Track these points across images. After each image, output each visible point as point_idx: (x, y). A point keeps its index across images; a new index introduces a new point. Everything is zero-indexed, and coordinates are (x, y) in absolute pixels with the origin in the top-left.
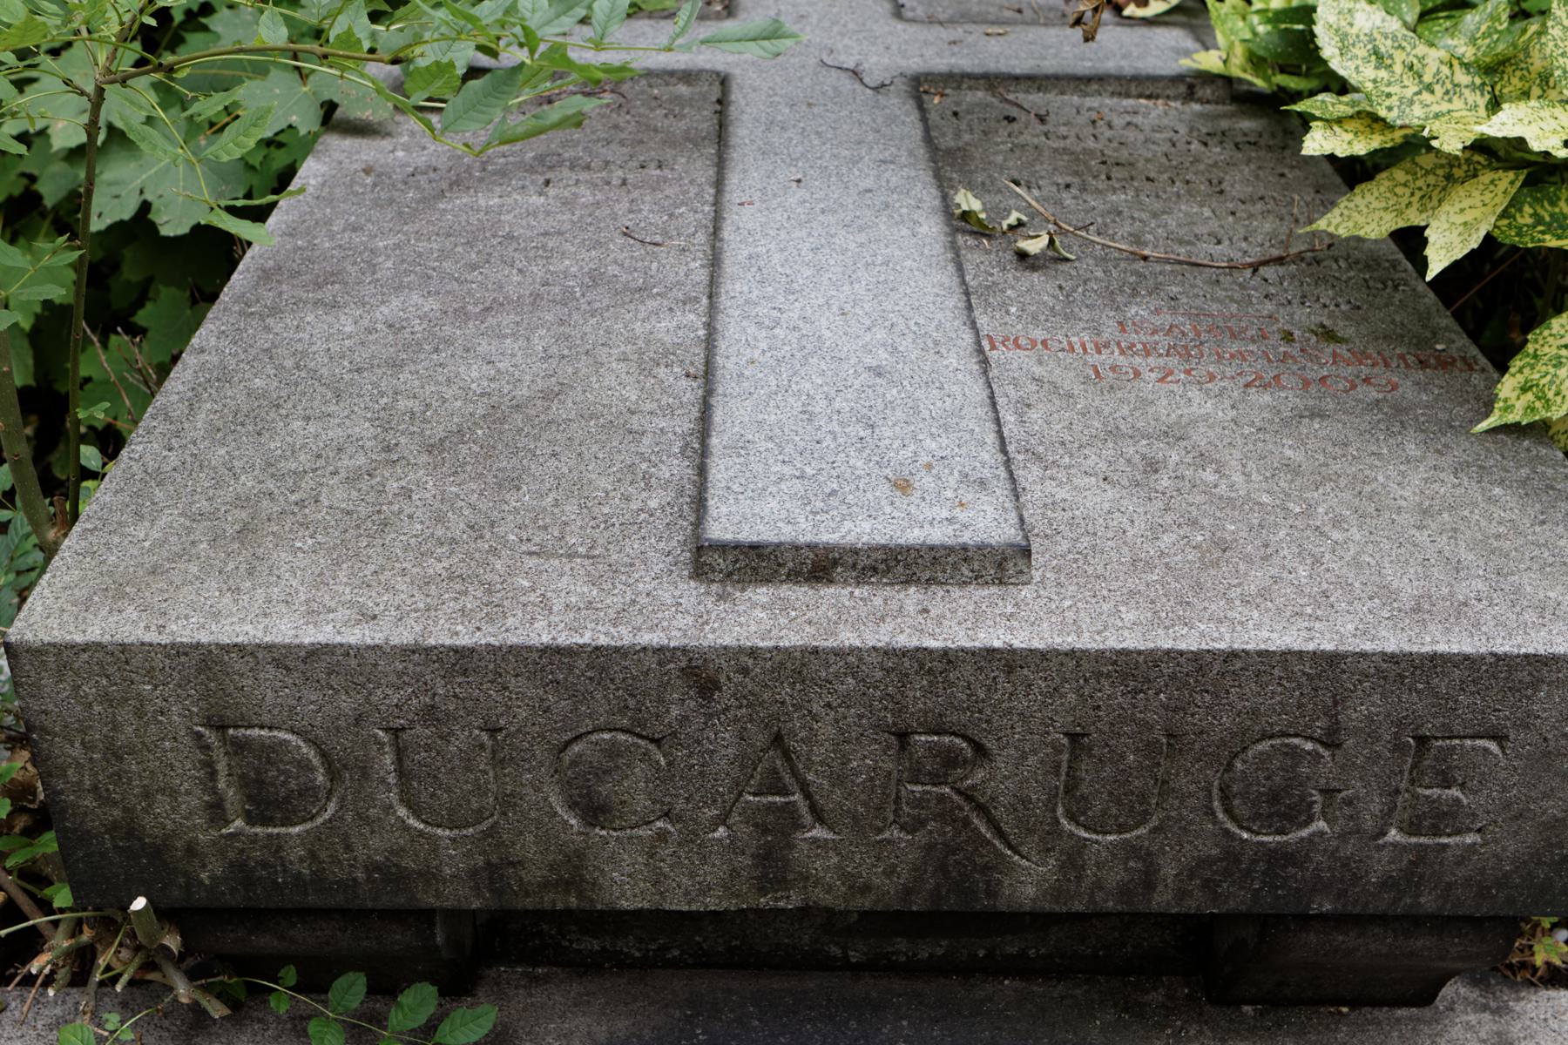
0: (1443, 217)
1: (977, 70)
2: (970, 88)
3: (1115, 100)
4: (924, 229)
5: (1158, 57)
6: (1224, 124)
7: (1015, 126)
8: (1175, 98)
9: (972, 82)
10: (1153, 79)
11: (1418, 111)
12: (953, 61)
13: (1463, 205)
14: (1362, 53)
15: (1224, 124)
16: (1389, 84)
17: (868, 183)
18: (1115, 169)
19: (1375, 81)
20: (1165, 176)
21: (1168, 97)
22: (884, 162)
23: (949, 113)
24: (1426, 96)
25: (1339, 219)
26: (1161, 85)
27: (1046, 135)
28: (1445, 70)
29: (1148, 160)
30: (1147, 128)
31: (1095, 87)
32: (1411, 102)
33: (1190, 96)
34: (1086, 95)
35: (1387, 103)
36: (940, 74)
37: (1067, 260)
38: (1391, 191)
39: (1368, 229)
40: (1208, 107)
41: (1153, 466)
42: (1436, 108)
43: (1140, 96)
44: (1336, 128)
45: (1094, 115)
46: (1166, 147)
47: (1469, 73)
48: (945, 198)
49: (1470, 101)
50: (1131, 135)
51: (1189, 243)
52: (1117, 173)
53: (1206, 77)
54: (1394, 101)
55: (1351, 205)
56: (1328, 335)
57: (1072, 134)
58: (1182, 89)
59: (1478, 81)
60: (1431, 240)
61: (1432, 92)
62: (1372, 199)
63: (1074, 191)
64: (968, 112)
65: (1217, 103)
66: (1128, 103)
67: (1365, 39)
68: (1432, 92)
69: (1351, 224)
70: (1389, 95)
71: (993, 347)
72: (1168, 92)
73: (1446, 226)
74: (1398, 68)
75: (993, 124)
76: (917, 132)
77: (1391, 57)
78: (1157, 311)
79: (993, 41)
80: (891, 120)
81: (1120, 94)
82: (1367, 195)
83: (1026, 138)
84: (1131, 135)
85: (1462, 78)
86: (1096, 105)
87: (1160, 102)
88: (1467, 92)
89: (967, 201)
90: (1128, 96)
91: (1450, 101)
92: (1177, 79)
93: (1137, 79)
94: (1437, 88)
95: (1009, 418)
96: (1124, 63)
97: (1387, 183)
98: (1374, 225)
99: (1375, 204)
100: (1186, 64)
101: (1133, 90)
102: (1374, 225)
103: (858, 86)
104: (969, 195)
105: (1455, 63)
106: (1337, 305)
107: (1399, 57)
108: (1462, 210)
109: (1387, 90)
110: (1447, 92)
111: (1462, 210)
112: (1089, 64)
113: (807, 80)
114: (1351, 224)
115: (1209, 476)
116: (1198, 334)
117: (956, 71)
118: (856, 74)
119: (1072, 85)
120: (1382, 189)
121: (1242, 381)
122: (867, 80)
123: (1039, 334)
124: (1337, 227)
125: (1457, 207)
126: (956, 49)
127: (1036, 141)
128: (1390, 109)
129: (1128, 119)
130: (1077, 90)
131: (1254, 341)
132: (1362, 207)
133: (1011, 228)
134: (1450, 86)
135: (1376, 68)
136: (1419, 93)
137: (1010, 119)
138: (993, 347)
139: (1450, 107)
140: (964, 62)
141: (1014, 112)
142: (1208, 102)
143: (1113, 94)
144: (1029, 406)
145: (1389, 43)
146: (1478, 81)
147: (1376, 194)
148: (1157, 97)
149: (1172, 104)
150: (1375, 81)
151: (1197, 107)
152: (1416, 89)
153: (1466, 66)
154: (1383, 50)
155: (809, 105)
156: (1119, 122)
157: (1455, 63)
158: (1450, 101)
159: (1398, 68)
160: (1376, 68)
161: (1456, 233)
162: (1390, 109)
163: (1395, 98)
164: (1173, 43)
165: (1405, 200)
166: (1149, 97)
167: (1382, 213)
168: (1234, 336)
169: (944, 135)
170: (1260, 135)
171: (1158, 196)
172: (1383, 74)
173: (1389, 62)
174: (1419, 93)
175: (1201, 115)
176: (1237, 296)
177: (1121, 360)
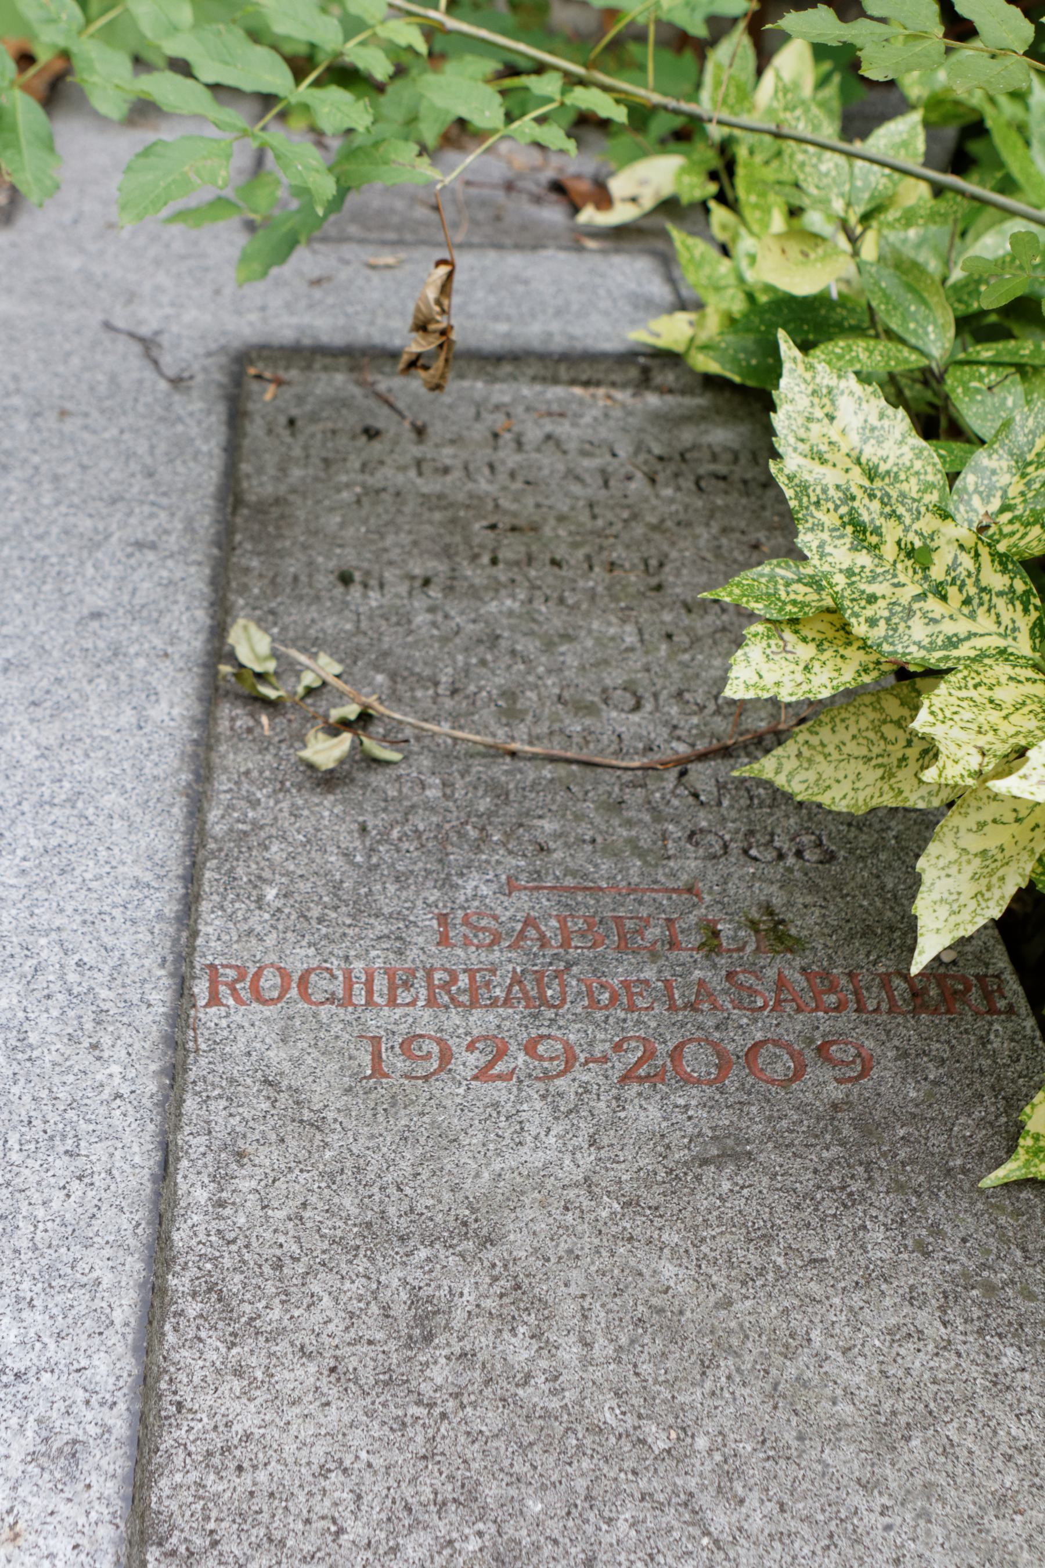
0: (949, 837)
1: (338, 340)
2: (325, 368)
3: (538, 388)
4: (158, 712)
5: (606, 314)
6: (687, 436)
7: (377, 446)
8: (624, 386)
9: (328, 361)
10: (592, 358)
11: (919, 631)
12: (307, 319)
13: (982, 816)
14: (830, 520)
15: (687, 436)
16: (873, 579)
17: (98, 598)
18: (511, 538)
19: (849, 573)
20: (580, 554)
21: (613, 384)
22: (140, 545)
23: (282, 420)
24: (932, 604)
25: (794, 763)
26: (602, 367)
27: (419, 463)
28: (967, 561)
29: (561, 519)
30: (572, 446)
31: (507, 368)
32: (910, 613)
33: (645, 382)
34: (494, 379)
35: (869, 612)
36: (282, 348)
37: (388, 763)
38: (877, 730)
39: (837, 792)
40: (670, 399)
41: (426, 1322)
42: (949, 628)
43: (573, 382)
44: (788, 635)
45: (499, 420)
46: (593, 490)
47: (1004, 571)
48: (219, 631)
49: (1006, 620)
50: (550, 463)
51: (591, 710)
52: (512, 549)
53: (670, 358)
54: (880, 609)
55: (814, 740)
56: (775, 933)
57: (458, 463)
58: (633, 373)
59: (1020, 586)
60: (927, 879)
61: (944, 598)
62: (847, 736)
63: (434, 592)
64: (314, 418)
65: (683, 392)
66: (556, 392)
67: (837, 495)
68: (944, 598)
69: (811, 776)
70: (872, 599)
71: (214, 999)
72: (614, 377)
73: (952, 855)
74: (889, 551)
75: (343, 441)
76: (208, 476)
77: (877, 531)
78: (511, 887)
79: (375, 277)
80: (180, 446)
81: (544, 380)
82: (841, 727)
83: (387, 475)
84: (550, 463)
85: (996, 580)
86: (506, 399)
87: (601, 391)
88: (1000, 603)
89: (251, 644)
90: (555, 381)
91: (972, 616)
92: (628, 357)
93: (567, 358)
94: (952, 591)
95: (194, 1189)
96: (555, 326)
97: (871, 715)
98: (846, 786)
99: (851, 748)
100: (639, 336)
101: (563, 372)
102: (846, 786)
103: (149, 374)
104: (253, 628)
105: (984, 551)
106: (799, 854)
107: (892, 532)
108: (981, 825)
109: (870, 589)
110: (967, 602)
111: (981, 825)
112: (503, 327)
113: (76, 361)
114: (811, 776)
115: (519, 1350)
116: (566, 944)
117: (307, 341)
118: (148, 346)
119: (474, 366)
120: (864, 723)
121: (619, 1066)
122: (166, 359)
123: (300, 958)
124: (791, 775)
125: (971, 822)
126: (317, 293)
127: (400, 479)
128: (872, 622)
129: (549, 427)
130: (480, 373)
131: (654, 956)
132: (830, 749)
133: (310, 691)
134: (972, 591)
135: (854, 549)
136: (922, 597)
137: (371, 434)
138: (214, 999)
139: (974, 628)
140: (325, 325)
141: (382, 418)
142: (671, 391)
143: (534, 379)
144: (240, 1155)
145: (875, 505)
146: (1020, 586)
147: (853, 730)
148: (598, 384)
149: (619, 395)
150: (849, 573)
151: (653, 400)
152: (918, 590)
153: (1002, 560)
154: (865, 517)
155: (63, 414)
156: (533, 434)
157: (984, 551)
158: (972, 616)
159: (889, 551)
160: (854, 549)
161: (969, 870)
162: (872, 622)
163: (881, 603)
164: (632, 286)
165: (897, 751)
166: (587, 384)
167: (860, 767)
168: (624, 945)
169: (260, 470)
170: (736, 460)
171: (561, 601)
172: (864, 559)
173: (874, 540)
174: (922, 597)
175: (658, 418)
176: (646, 840)
177: (425, 1020)
